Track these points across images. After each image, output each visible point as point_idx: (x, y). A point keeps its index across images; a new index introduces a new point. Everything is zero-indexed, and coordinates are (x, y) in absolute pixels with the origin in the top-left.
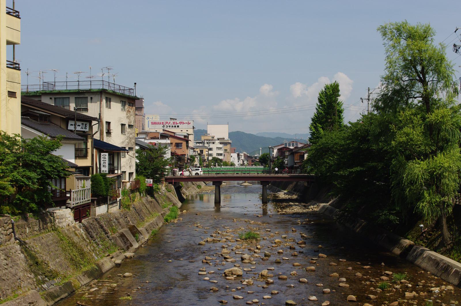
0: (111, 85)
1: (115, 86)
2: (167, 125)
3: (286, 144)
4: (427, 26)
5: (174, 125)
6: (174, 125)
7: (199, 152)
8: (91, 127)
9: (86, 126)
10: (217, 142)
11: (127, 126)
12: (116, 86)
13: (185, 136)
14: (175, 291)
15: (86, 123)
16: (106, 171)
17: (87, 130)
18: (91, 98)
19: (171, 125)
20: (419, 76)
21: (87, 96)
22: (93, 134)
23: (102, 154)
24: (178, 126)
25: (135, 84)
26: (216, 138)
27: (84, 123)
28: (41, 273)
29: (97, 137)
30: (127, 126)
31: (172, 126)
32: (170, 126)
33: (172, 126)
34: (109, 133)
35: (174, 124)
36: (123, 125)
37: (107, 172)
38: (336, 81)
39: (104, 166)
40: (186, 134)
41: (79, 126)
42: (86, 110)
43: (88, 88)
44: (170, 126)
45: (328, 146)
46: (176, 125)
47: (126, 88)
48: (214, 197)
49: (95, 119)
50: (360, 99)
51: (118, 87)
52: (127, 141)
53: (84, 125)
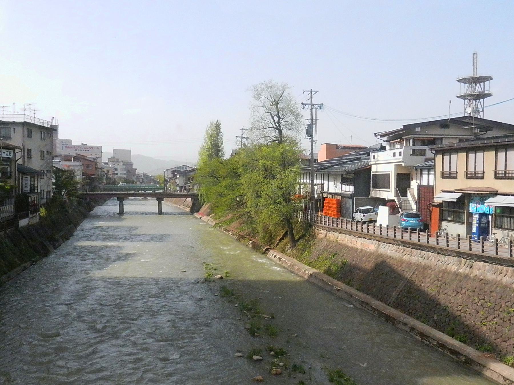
0: (32, 118)
1: (36, 119)
2: (79, 149)
3: (178, 167)
4: (279, 93)
5: (85, 149)
6: (85, 149)
7: (106, 172)
8: (15, 154)
9: (10, 153)
10: (121, 163)
11: (45, 153)
12: (36, 119)
13: (94, 159)
14: (71, 282)
15: (11, 151)
16: (27, 191)
17: (11, 156)
18: (14, 129)
19: (82, 150)
20: (276, 125)
21: (10, 127)
22: (17, 159)
23: (24, 176)
24: (88, 151)
25: (53, 118)
26: (120, 160)
27: (9, 151)
28: (43, 283)
29: (20, 162)
30: (45, 153)
31: (83, 150)
32: (81, 150)
33: (83, 150)
34: (29, 157)
35: (85, 148)
36: (42, 152)
37: (29, 192)
38: (217, 121)
39: (26, 187)
40: (94, 157)
41: (5, 153)
42: (9, 138)
43: (11, 120)
44: (81, 150)
45: (222, 326)
46: (87, 149)
47: (44, 121)
48: (119, 207)
49: (19, 148)
50: (235, 137)
51: (38, 120)
52: (45, 165)
53: (9, 152)
